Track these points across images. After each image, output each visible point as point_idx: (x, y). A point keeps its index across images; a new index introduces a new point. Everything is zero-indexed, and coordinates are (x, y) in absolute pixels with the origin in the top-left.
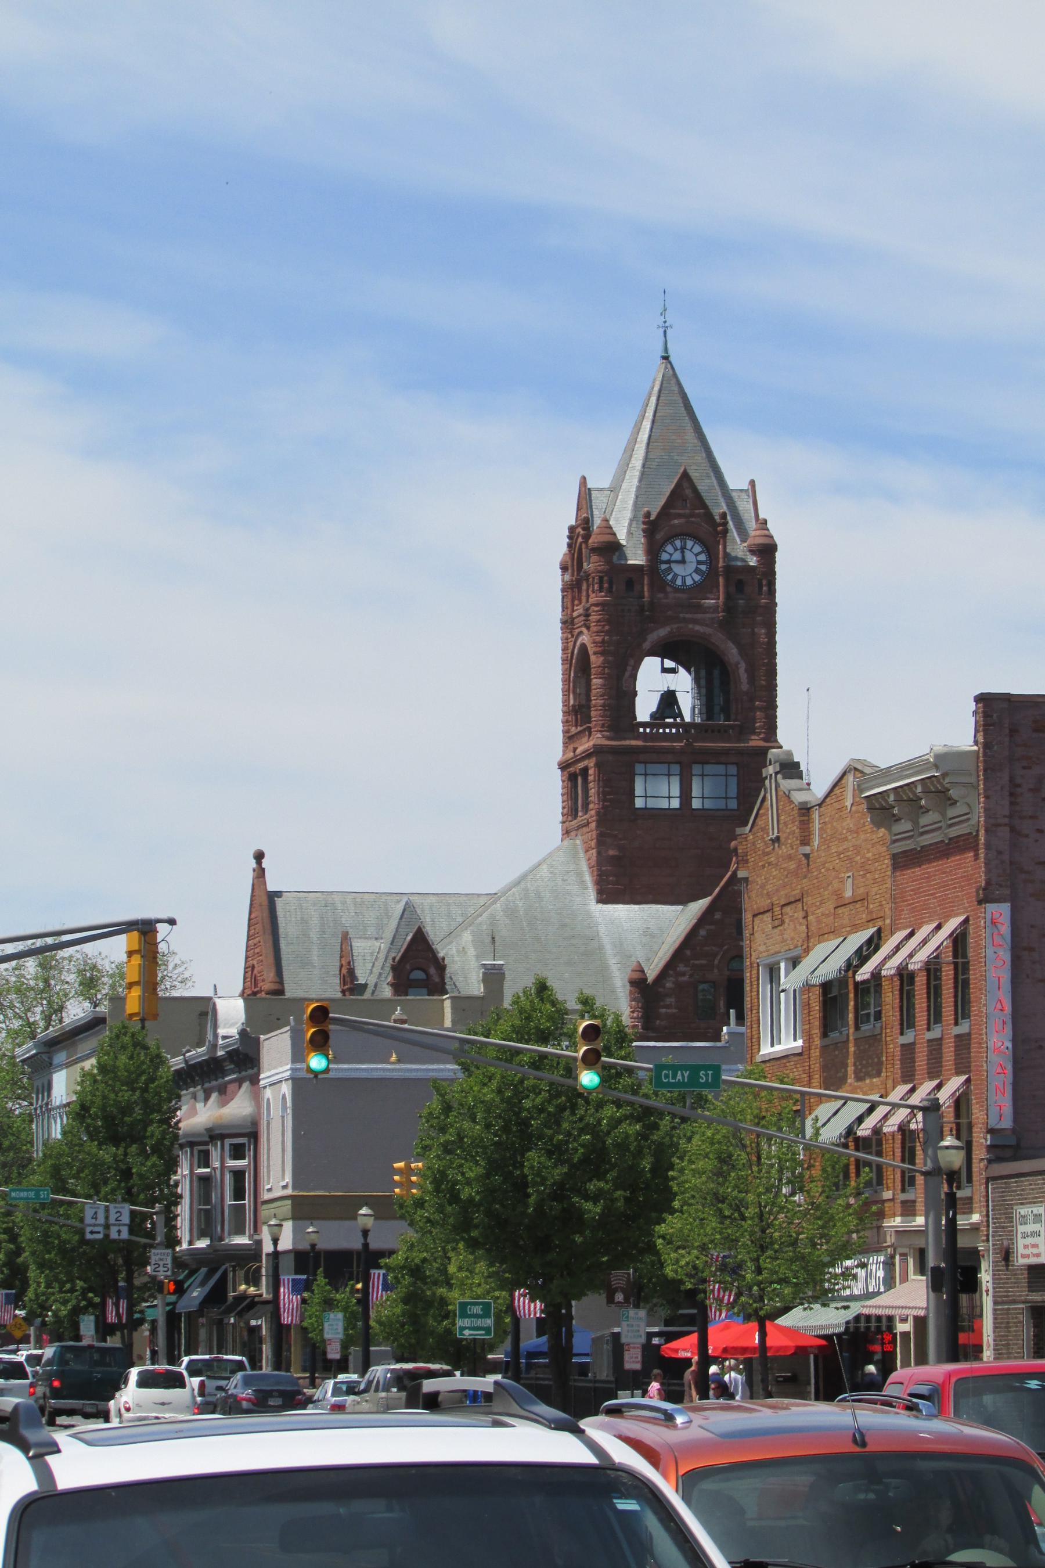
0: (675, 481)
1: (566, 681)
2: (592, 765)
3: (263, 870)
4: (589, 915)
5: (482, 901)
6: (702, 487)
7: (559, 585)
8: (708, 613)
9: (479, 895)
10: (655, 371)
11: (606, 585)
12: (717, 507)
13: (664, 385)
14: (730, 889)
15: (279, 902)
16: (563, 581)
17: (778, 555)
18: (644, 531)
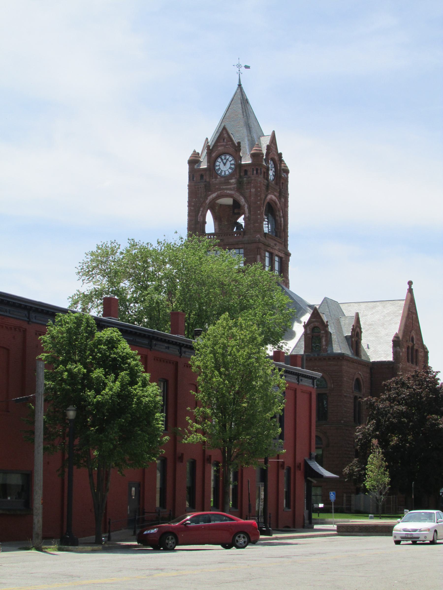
3: (412, 289)
8: (232, 185)
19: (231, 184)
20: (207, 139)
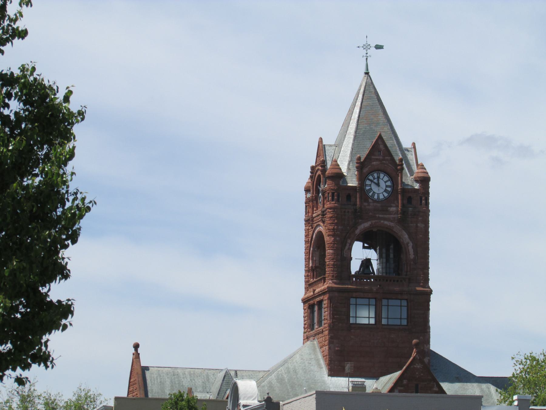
0: (374, 141)
1: (307, 253)
2: (326, 298)
4: (324, 382)
5: (261, 375)
6: (389, 144)
7: (304, 200)
8: (392, 214)
9: (259, 371)
10: (359, 80)
11: (335, 197)
12: (398, 156)
13: (366, 88)
14: (412, 367)
15: (148, 373)
16: (306, 197)
17: (431, 184)
18: (357, 167)
19: (390, 213)
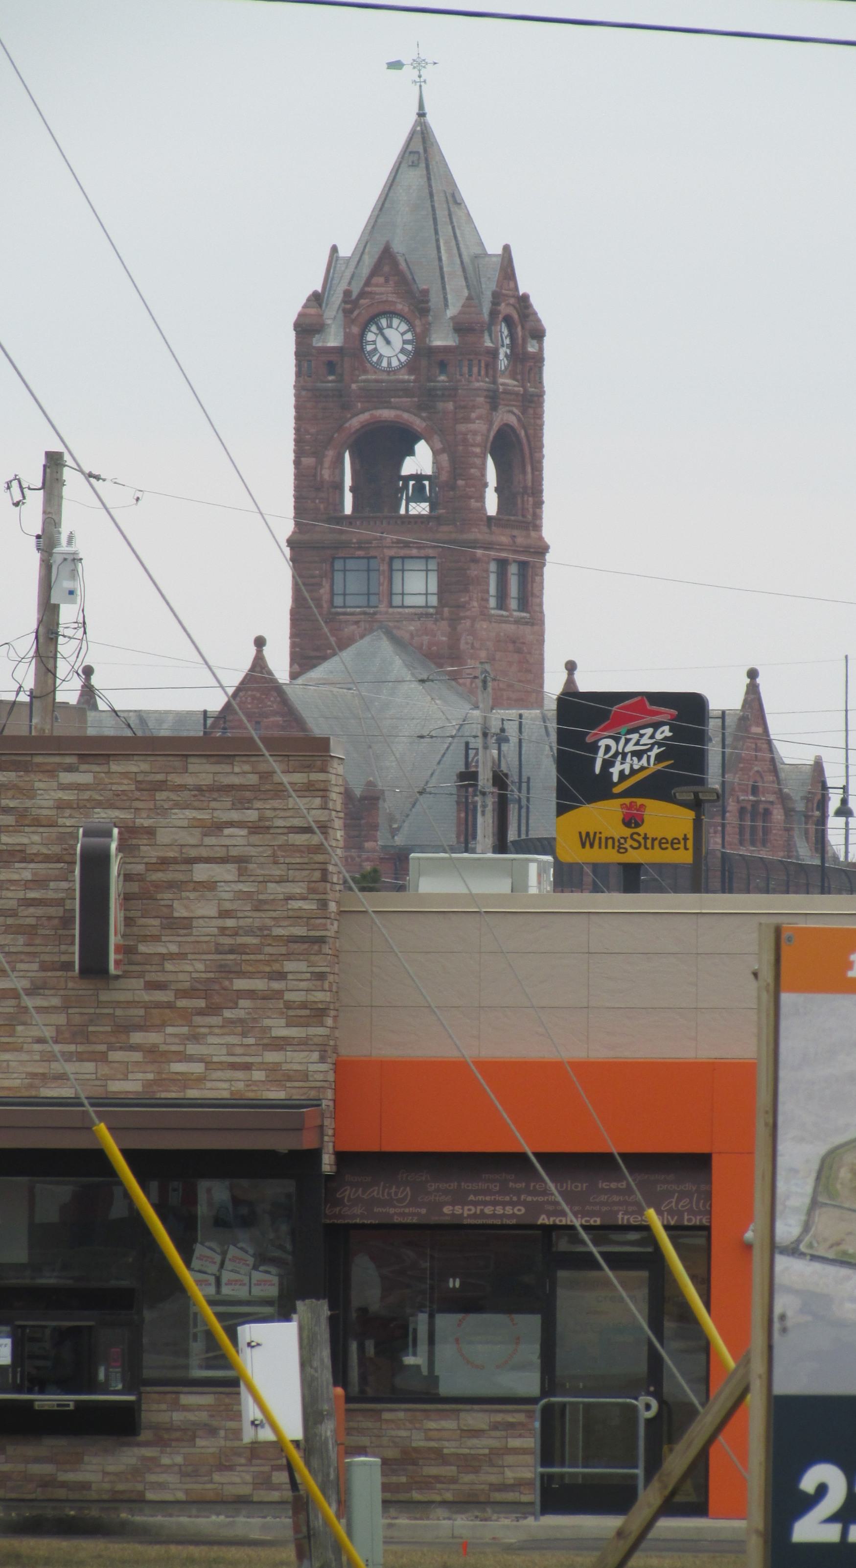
20: (334, 249)
